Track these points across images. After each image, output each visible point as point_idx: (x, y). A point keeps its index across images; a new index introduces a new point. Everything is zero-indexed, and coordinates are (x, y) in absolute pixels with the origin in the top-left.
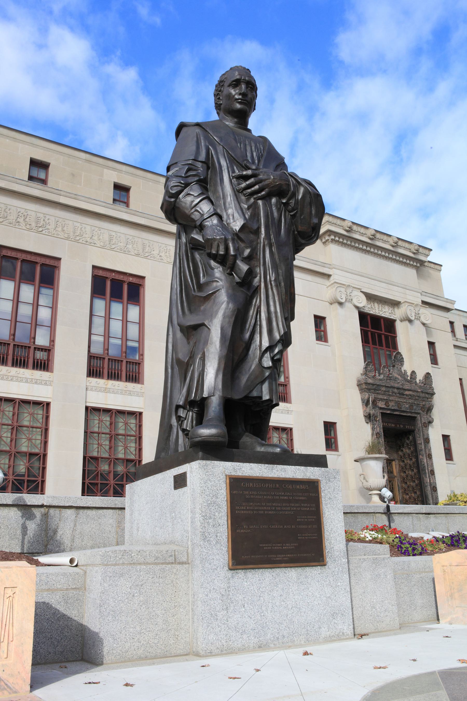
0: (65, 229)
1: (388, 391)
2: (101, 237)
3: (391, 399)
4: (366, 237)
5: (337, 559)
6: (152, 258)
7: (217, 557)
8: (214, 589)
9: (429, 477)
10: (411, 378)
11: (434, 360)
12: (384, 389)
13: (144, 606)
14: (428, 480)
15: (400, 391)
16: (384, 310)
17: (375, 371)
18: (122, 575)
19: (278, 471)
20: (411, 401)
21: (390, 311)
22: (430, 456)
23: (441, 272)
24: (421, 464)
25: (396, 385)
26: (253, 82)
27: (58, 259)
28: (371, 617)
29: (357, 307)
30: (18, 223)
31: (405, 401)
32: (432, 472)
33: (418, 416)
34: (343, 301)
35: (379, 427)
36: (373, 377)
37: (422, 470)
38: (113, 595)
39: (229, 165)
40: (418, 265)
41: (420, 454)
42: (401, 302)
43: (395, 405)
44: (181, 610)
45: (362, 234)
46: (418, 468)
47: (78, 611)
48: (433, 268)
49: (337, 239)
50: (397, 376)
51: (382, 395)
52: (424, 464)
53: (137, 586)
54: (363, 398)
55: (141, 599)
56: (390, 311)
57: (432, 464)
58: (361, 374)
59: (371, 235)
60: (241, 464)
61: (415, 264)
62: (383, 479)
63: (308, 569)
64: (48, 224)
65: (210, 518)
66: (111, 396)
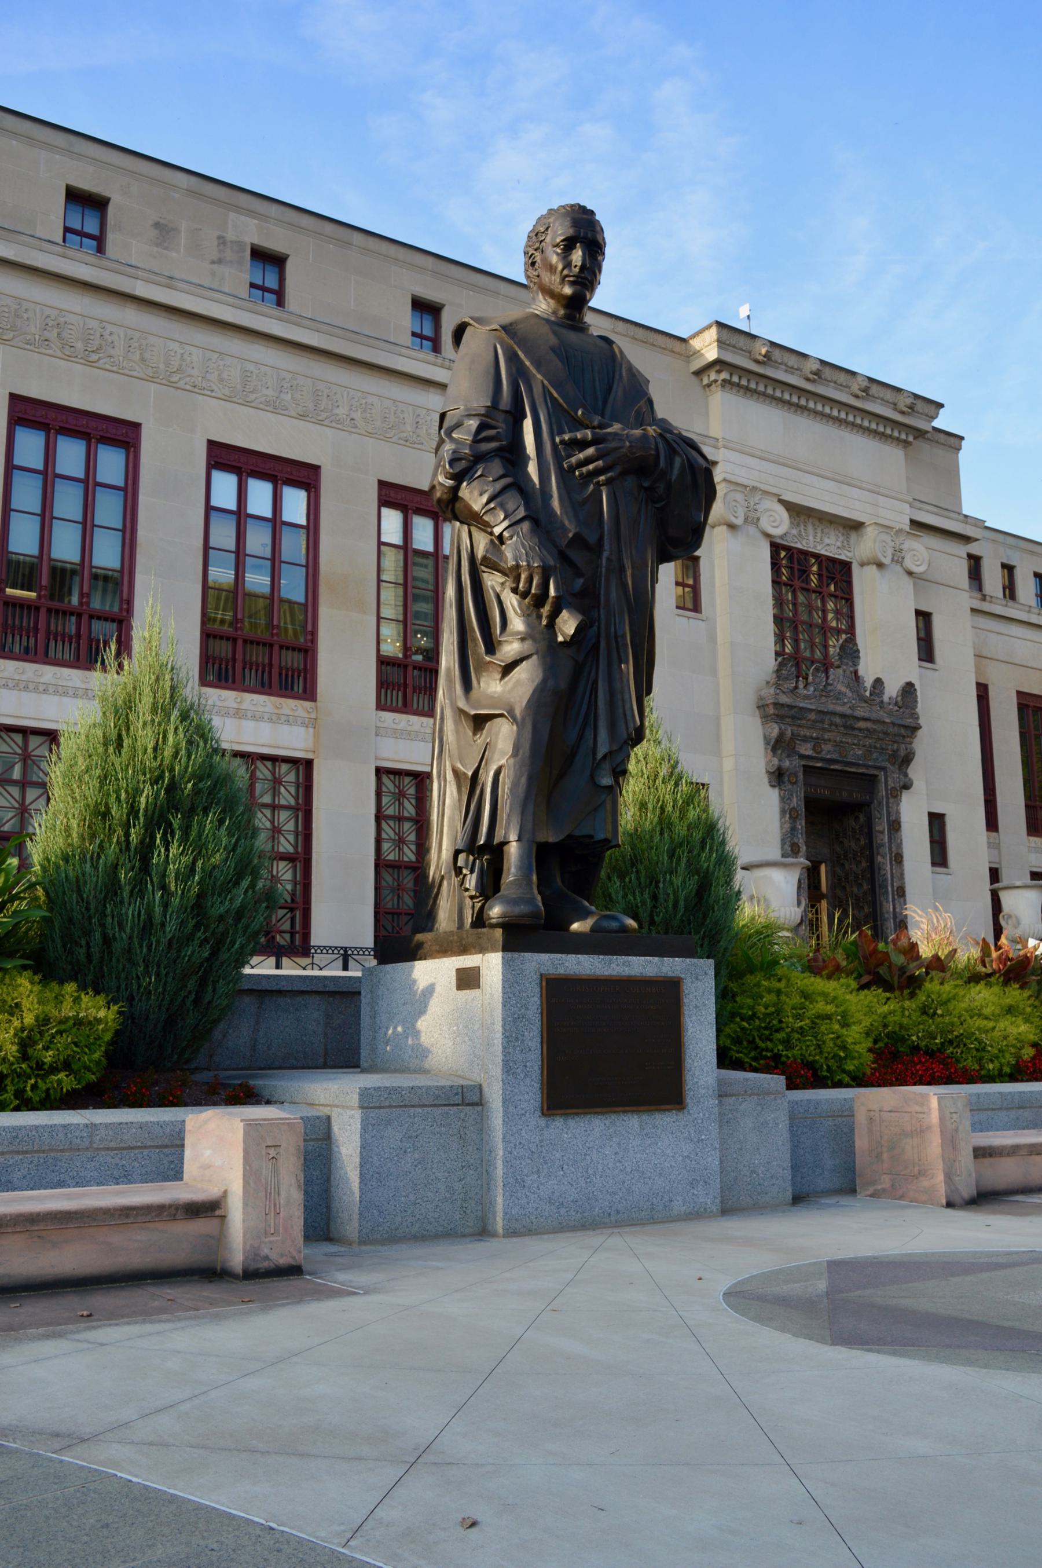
0: (147, 355)
1: (822, 722)
2: (225, 376)
3: (826, 737)
4: (800, 376)
5: (702, 1100)
6: (334, 424)
7: (526, 1096)
8: (520, 1143)
9: (894, 900)
10: (871, 694)
11: (926, 651)
12: (813, 716)
13: (420, 1166)
14: (891, 907)
15: (846, 722)
16: (827, 541)
17: (798, 677)
18: (389, 1122)
19: (618, 965)
20: (868, 742)
21: (839, 544)
22: (898, 859)
23: (961, 454)
24: (879, 873)
25: (839, 709)
26: (601, 242)
27: (136, 426)
28: (749, 1187)
29: (767, 535)
30: (46, 343)
31: (856, 742)
32: (901, 892)
33: (882, 775)
34: (739, 521)
35: (797, 797)
36: (792, 691)
37: (880, 886)
38: (378, 1151)
39: (551, 410)
40: (911, 439)
41: (878, 854)
42: (864, 523)
43: (835, 751)
44: (471, 1172)
45: (791, 370)
46: (872, 881)
47: (321, 1171)
48: (943, 444)
49: (735, 379)
50: (843, 689)
51: (809, 728)
52: (884, 875)
53: (410, 1137)
54: (767, 734)
55: (416, 1156)
56: (839, 544)
57: (902, 874)
58: (768, 683)
59: (811, 373)
60: (563, 956)
61: (903, 436)
62: (796, 909)
63: (658, 1116)
64: (112, 345)
65: (517, 1039)
66: (249, 725)
